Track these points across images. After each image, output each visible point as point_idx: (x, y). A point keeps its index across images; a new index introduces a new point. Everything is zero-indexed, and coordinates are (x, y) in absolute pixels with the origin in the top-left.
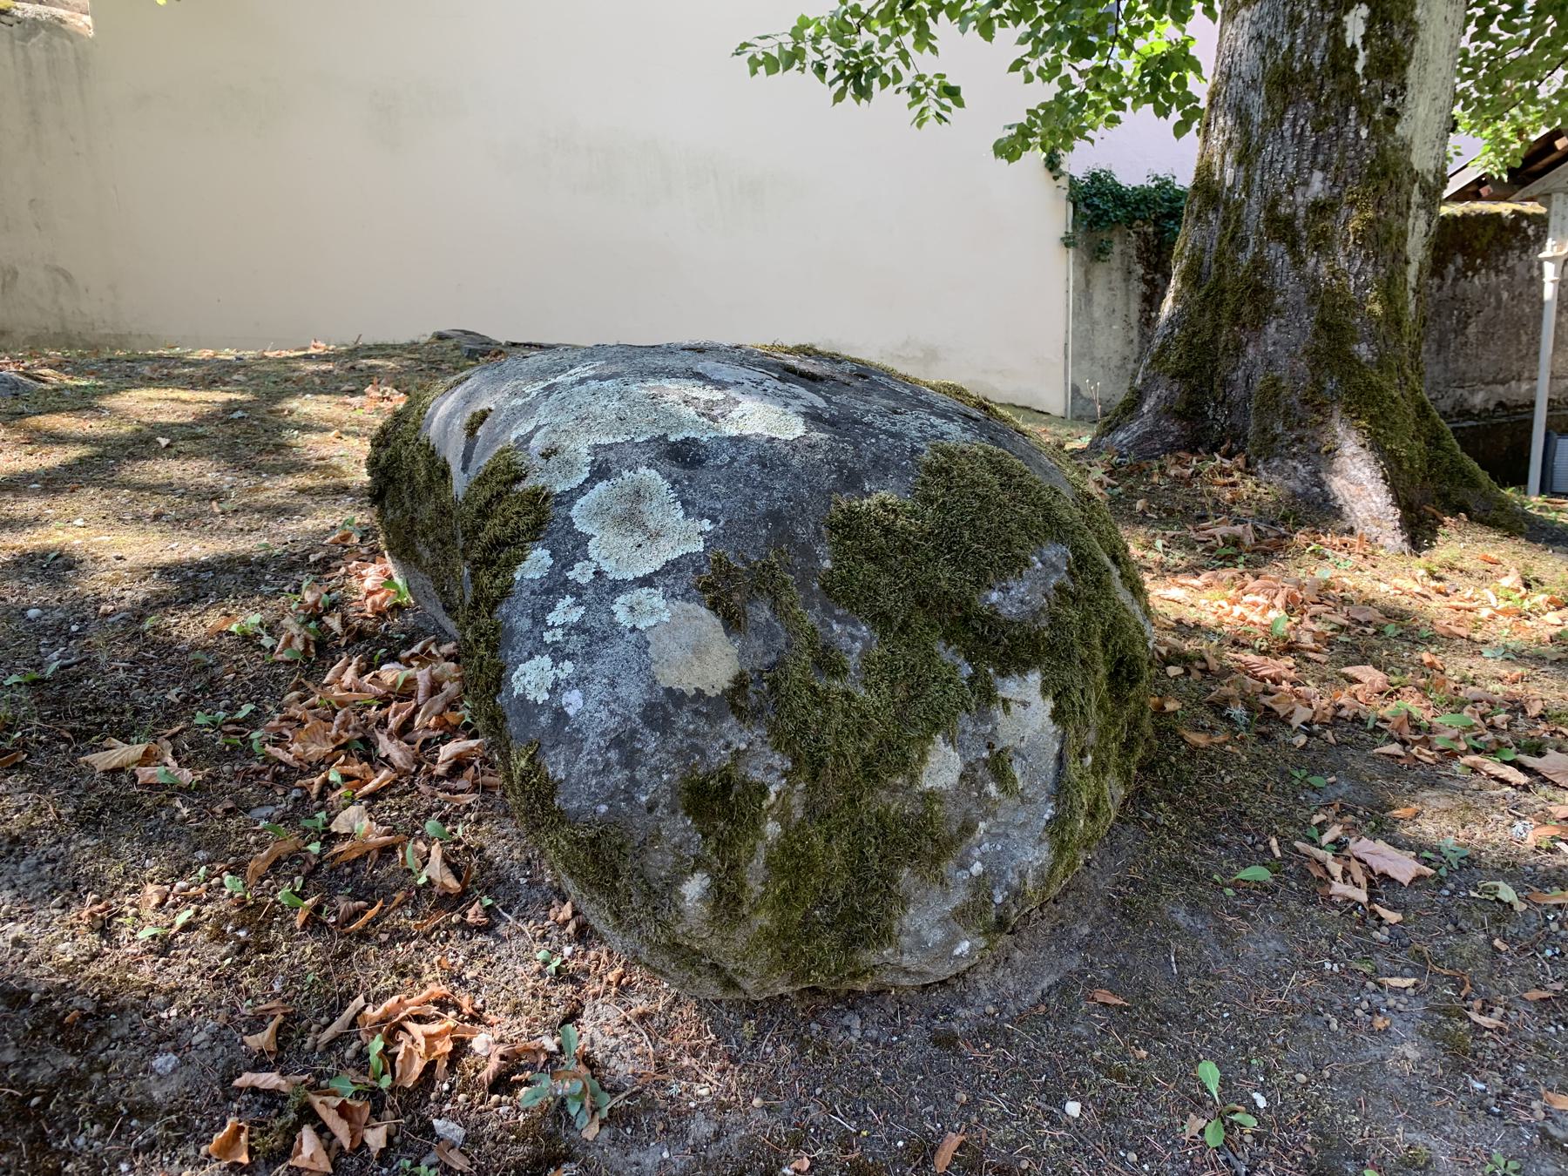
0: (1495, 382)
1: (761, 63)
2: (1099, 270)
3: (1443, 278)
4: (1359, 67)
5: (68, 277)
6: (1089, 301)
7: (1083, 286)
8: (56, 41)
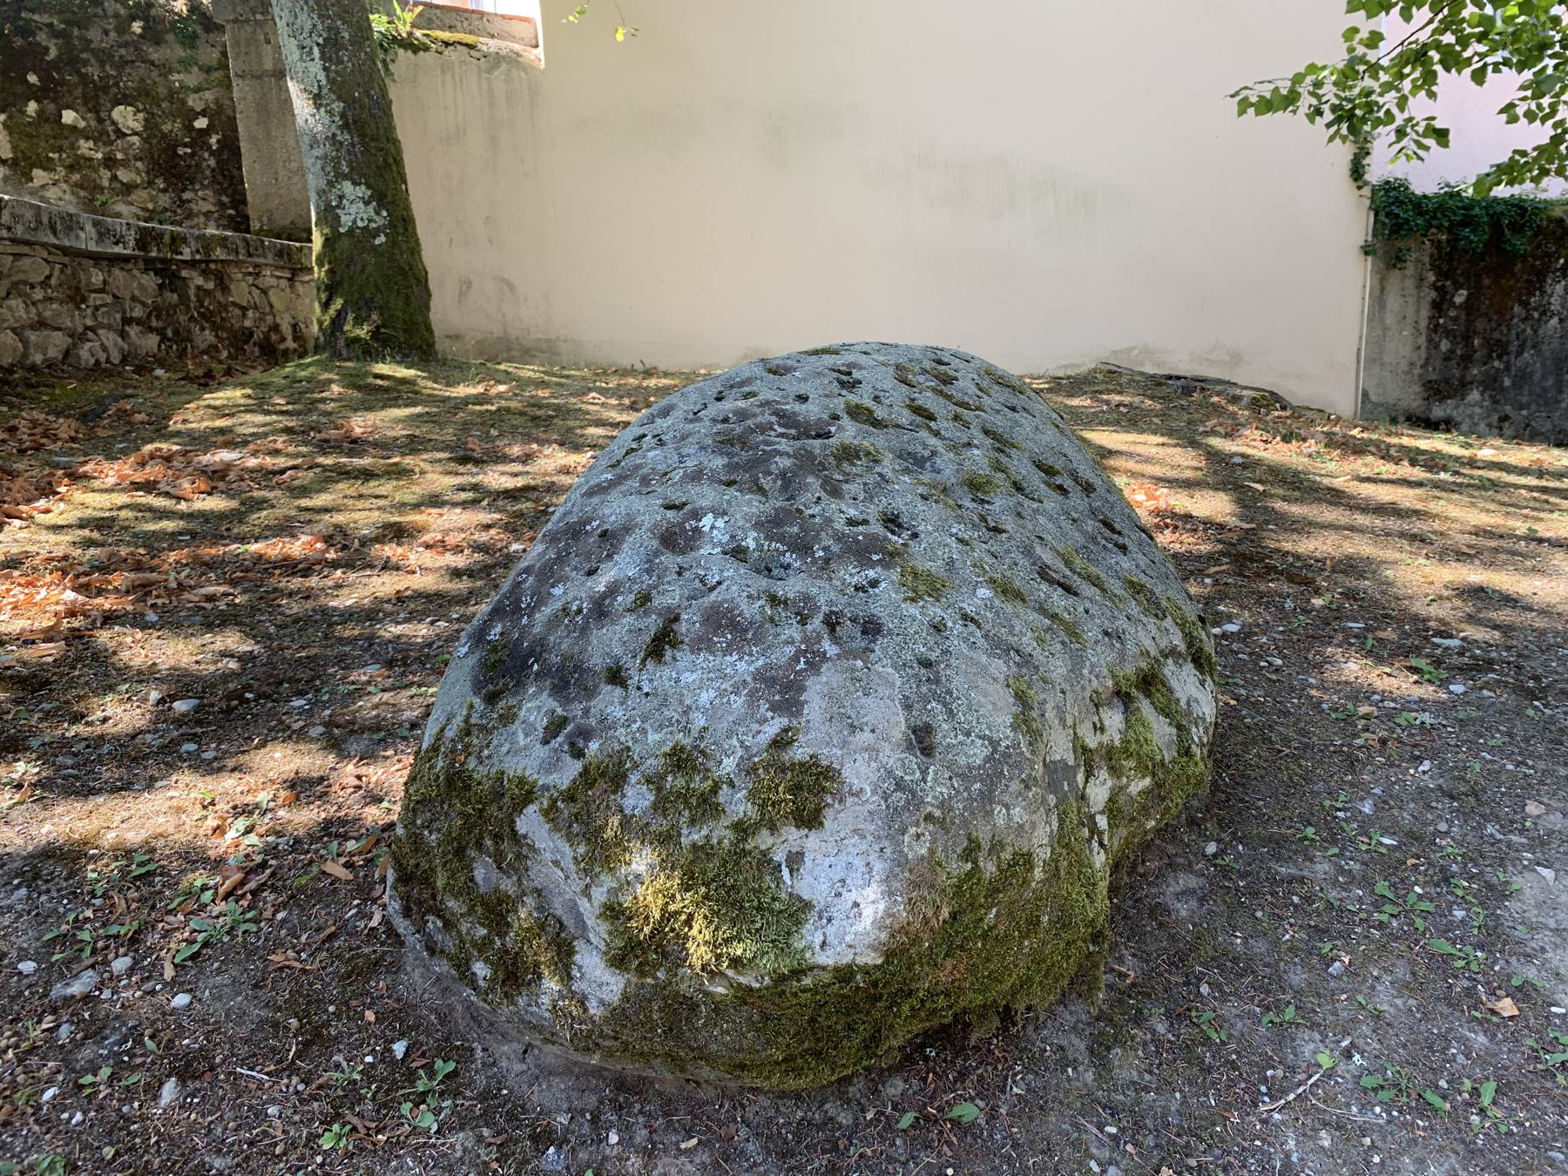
1: (1252, 105)
2: (1394, 277)
5: (511, 287)
8: (514, 72)
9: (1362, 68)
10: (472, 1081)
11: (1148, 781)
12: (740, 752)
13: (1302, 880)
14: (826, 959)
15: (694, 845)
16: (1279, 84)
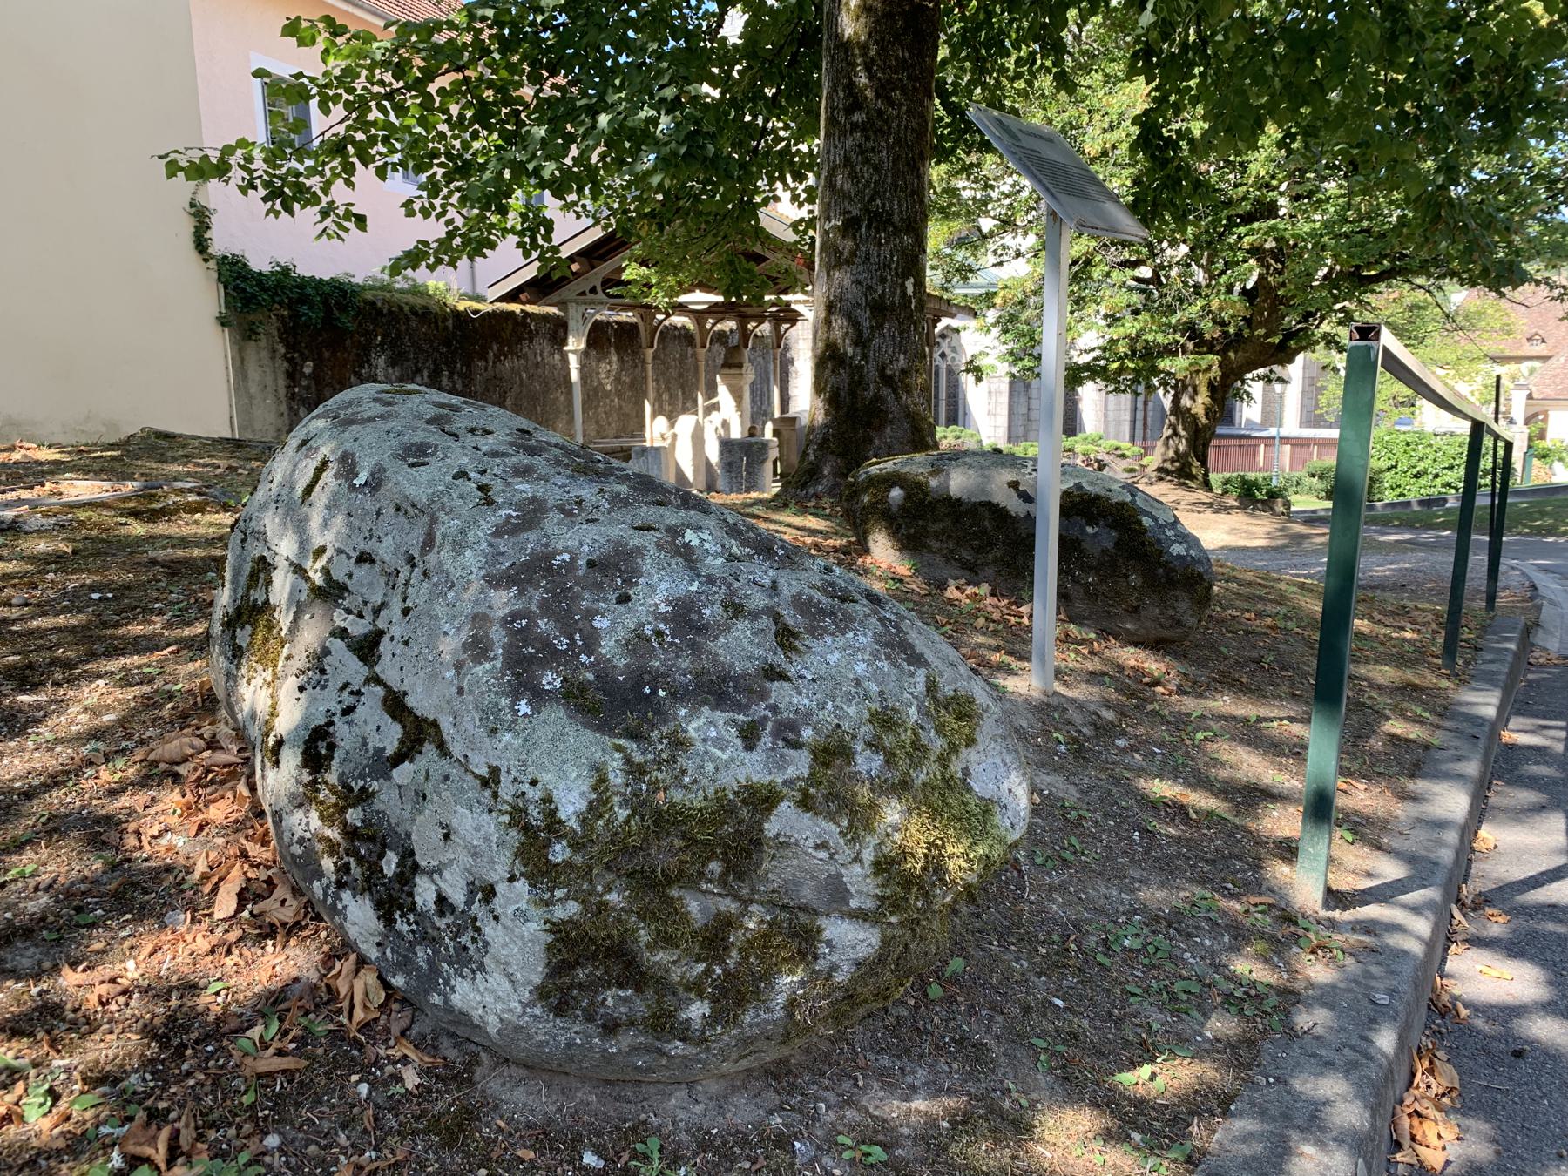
7: (238, 363)
9: (289, 151)
10: (679, 1144)
15: (924, 784)
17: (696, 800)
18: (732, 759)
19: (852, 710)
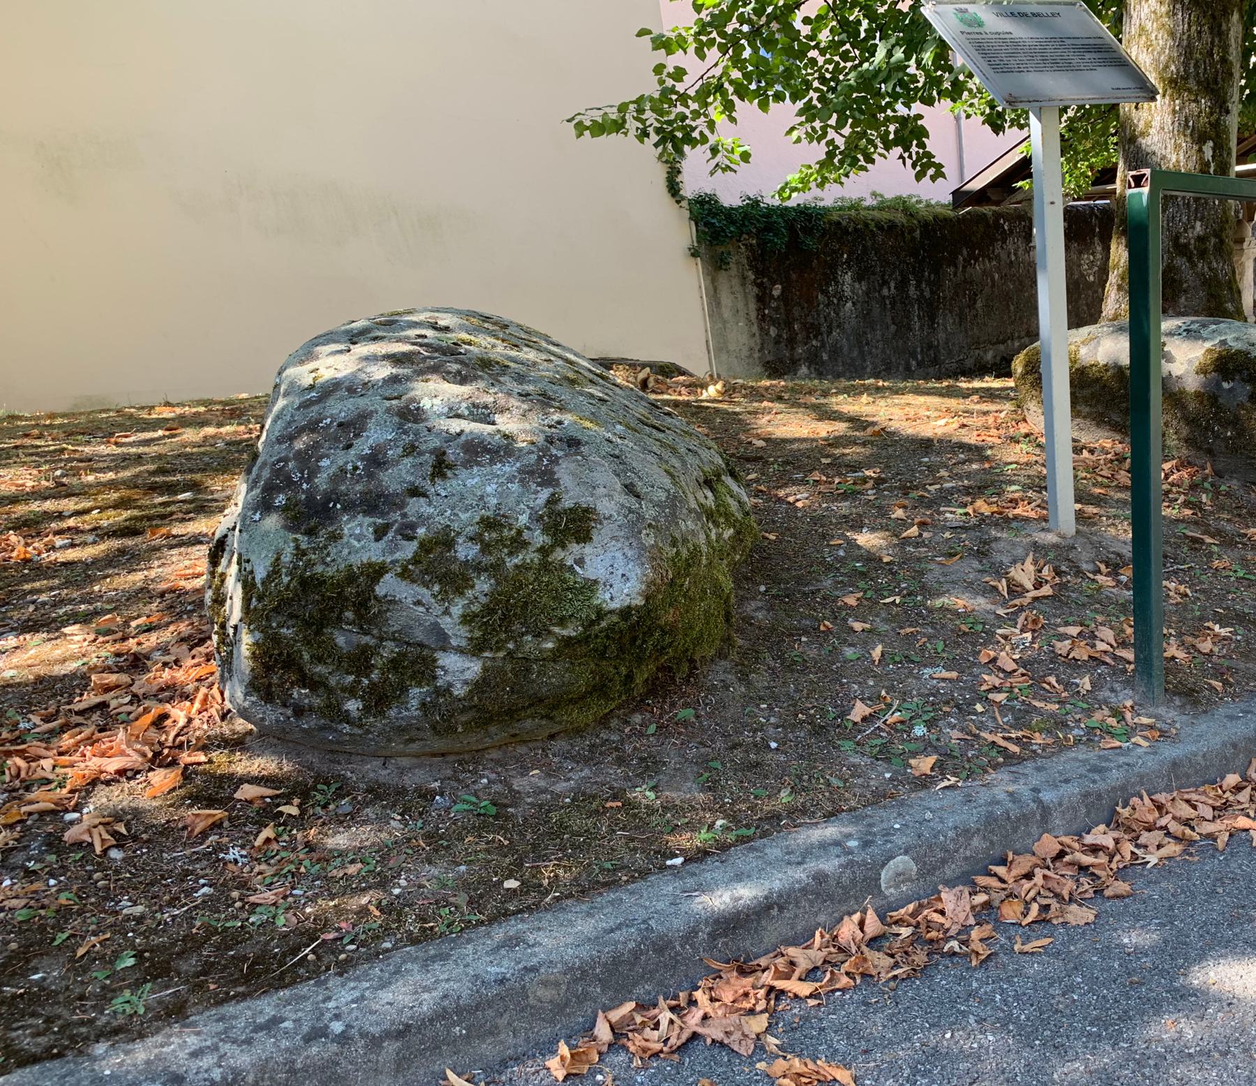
0: (998, 342)
1: (587, 128)
3: (956, 267)
4: (1212, 171)
6: (718, 304)
9: (674, 97)
11: (732, 530)
12: (528, 511)
13: (819, 590)
14: (615, 605)
15: (517, 566)
16: (608, 110)
17: (330, 572)
18: (363, 547)
19: (463, 516)
